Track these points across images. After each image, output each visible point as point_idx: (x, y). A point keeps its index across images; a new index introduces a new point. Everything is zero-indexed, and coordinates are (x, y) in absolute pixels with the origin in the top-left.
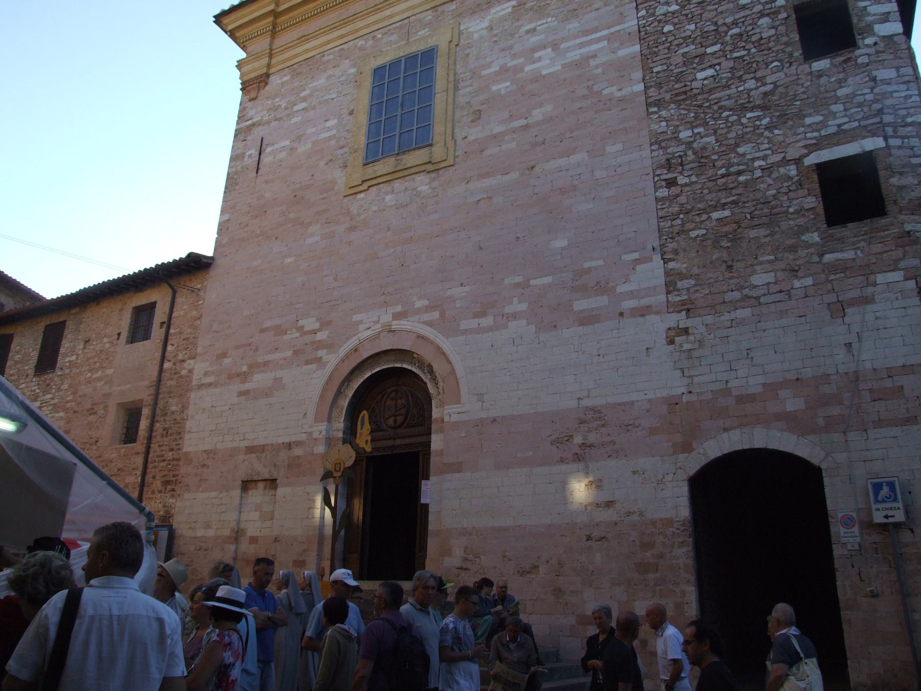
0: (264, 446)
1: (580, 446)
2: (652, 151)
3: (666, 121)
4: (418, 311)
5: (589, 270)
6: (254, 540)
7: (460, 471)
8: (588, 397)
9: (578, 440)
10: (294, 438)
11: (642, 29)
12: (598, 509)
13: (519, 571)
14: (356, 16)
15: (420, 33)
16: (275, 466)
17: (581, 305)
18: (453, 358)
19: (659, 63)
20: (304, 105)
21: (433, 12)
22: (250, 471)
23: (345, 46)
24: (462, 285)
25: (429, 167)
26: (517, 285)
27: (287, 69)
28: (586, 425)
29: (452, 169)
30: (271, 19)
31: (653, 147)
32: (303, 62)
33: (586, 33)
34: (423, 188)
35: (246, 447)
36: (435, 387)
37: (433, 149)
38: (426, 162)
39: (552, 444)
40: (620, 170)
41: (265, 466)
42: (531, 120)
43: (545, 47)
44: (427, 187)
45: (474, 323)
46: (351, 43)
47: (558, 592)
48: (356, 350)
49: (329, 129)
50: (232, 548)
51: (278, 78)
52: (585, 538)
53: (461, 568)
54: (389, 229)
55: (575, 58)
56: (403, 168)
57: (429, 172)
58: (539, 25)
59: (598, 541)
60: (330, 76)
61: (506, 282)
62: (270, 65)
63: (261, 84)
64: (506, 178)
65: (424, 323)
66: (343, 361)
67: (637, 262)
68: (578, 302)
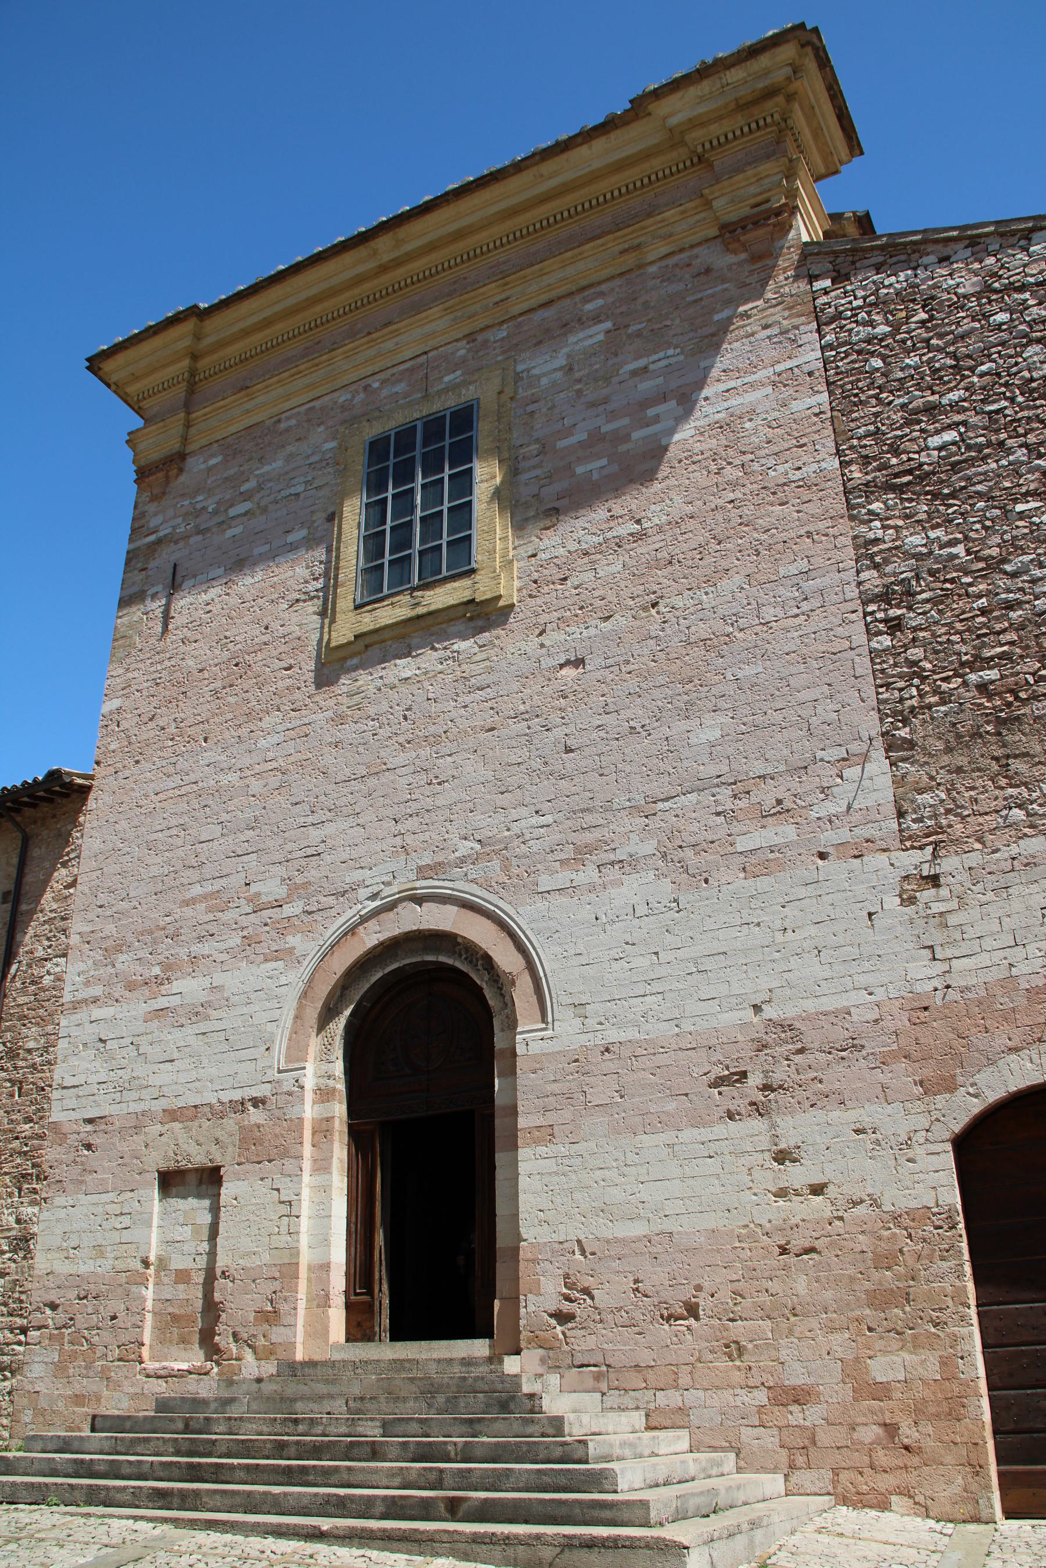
15: (446, 379)
20: (247, 506)
21: (468, 343)
23: (317, 404)
45: (563, 878)
46: (326, 398)
58: (653, 363)
62: (186, 439)
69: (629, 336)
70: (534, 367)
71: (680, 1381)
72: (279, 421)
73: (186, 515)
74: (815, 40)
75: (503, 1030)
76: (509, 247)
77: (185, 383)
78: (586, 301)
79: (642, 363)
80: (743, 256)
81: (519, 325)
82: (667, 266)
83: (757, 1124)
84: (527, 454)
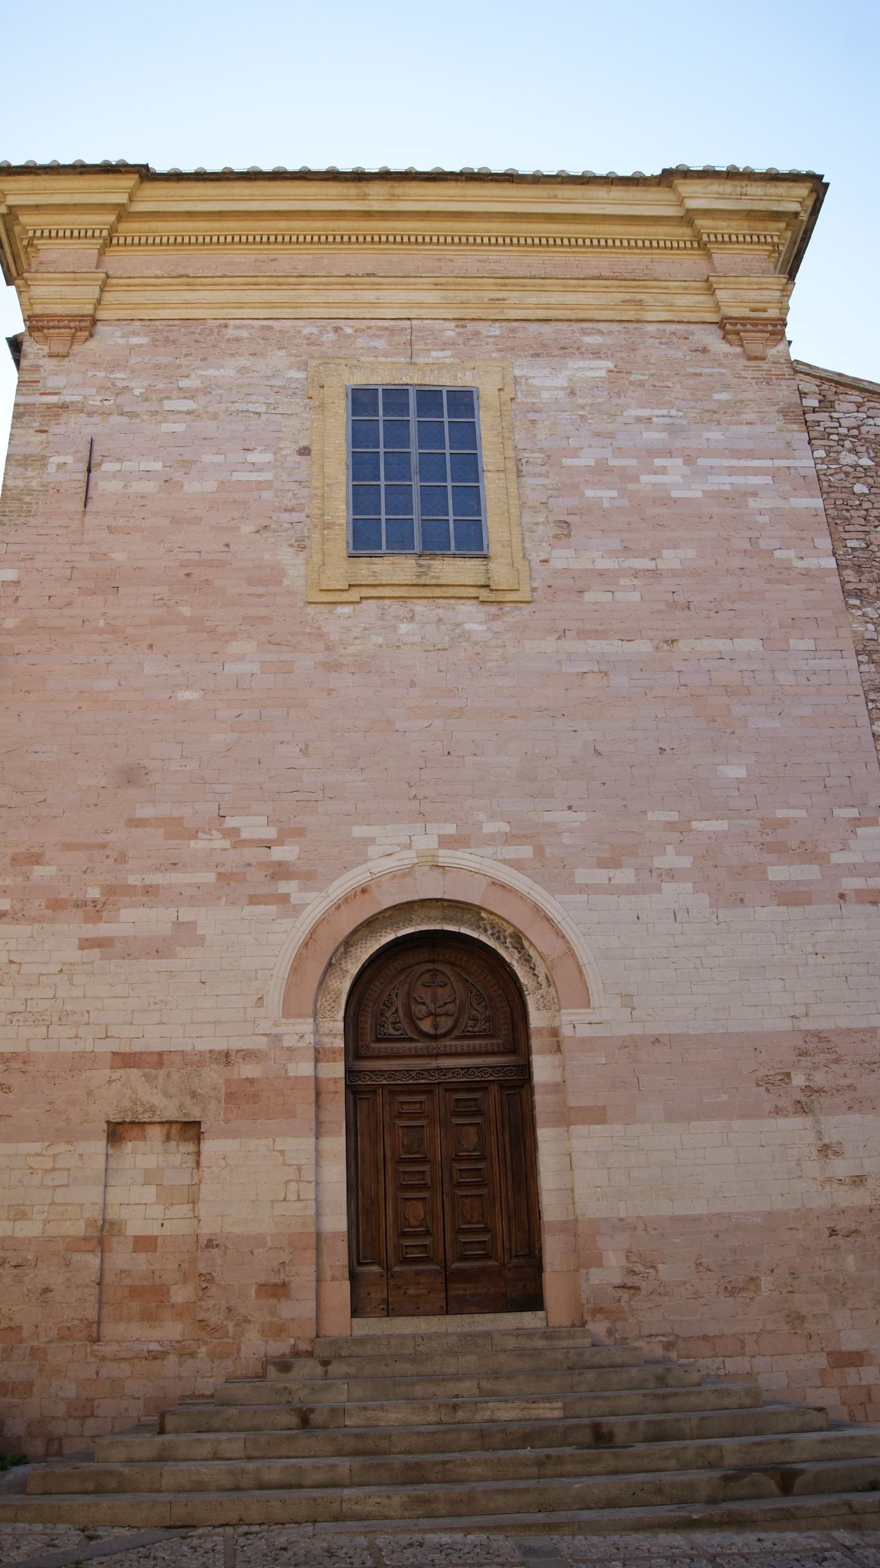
0: (160, 1054)
1: (802, 1090)
2: (860, 663)
3: (874, 624)
4: (491, 840)
5: (785, 823)
6: (146, 1244)
7: (603, 1121)
8: (806, 1015)
9: (798, 1080)
10: (234, 1044)
11: (822, 477)
12: (842, 1187)
13: (726, 1288)
14: (304, 279)
15: (434, 354)
16: (194, 1095)
17: (778, 873)
18: (566, 928)
19: (854, 535)
20: (189, 405)
21: (457, 326)
22: (127, 1104)
23: (275, 324)
24: (570, 808)
25: (484, 594)
26: (670, 826)
27: (139, 323)
28: (808, 1058)
29: (527, 609)
30: (112, 218)
31: (860, 658)
32: (177, 322)
33: (737, 454)
34: (474, 627)
35: (114, 1054)
36: (530, 975)
37: (491, 565)
38: (479, 583)
39: (758, 1085)
40: (815, 680)
41: (169, 1096)
42: (662, 565)
43: (670, 454)
44: (483, 628)
45: (600, 876)
46: (288, 323)
47: (796, 1319)
48: (364, 891)
49: (254, 467)
50: (94, 1261)
51: (118, 334)
52: (827, 1233)
53: (624, 1286)
54: (413, 684)
55: (723, 487)
56: (433, 582)
57: (483, 602)
58: (658, 416)
59: (847, 1236)
60: (243, 370)
61: (651, 816)
62: (99, 304)
63: (79, 334)
64: (628, 647)
65: (505, 862)
66: (339, 907)
67: (857, 822)
68: (774, 868)
69: (632, 383)
70: (533, 377)
71: (747, 1349)
72: (226, 326)
73: (101, 388)
74: (821, 193)
75: (538, 1009)
76: (502, 248)
77: (101, 241)
78: (583, 332)
79: (646, 412)
80: (738, 350)
81: (513, 330)
82: (664, 331)
83: (805, 1122)
84: (531, 460)
